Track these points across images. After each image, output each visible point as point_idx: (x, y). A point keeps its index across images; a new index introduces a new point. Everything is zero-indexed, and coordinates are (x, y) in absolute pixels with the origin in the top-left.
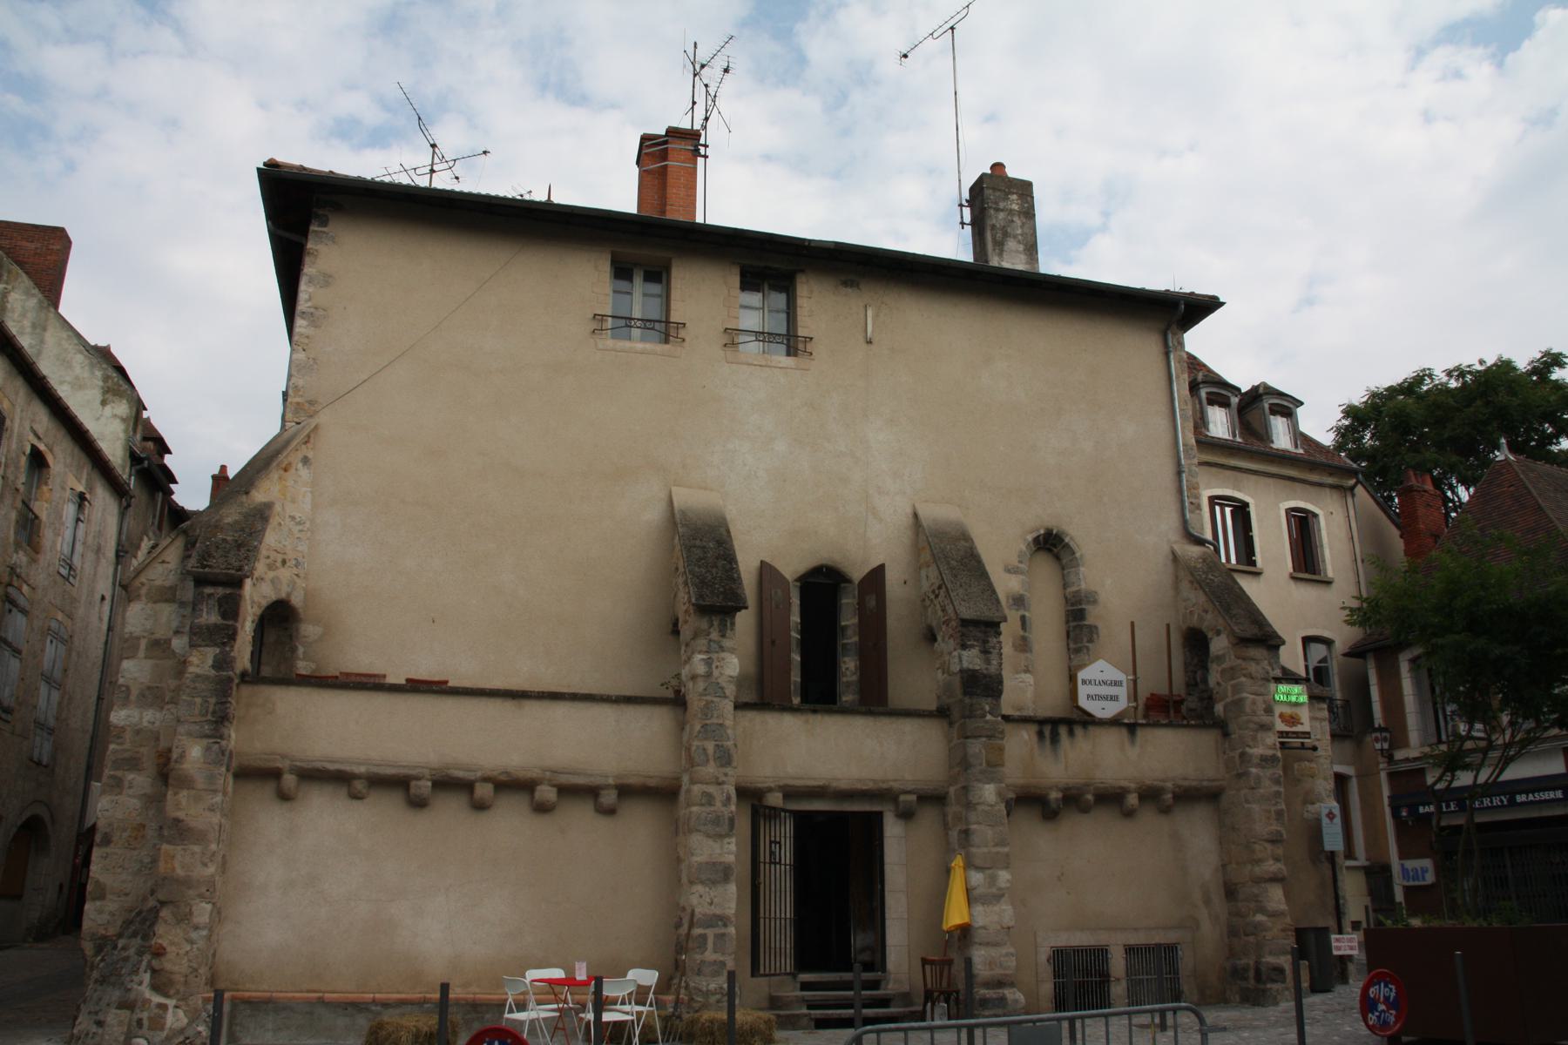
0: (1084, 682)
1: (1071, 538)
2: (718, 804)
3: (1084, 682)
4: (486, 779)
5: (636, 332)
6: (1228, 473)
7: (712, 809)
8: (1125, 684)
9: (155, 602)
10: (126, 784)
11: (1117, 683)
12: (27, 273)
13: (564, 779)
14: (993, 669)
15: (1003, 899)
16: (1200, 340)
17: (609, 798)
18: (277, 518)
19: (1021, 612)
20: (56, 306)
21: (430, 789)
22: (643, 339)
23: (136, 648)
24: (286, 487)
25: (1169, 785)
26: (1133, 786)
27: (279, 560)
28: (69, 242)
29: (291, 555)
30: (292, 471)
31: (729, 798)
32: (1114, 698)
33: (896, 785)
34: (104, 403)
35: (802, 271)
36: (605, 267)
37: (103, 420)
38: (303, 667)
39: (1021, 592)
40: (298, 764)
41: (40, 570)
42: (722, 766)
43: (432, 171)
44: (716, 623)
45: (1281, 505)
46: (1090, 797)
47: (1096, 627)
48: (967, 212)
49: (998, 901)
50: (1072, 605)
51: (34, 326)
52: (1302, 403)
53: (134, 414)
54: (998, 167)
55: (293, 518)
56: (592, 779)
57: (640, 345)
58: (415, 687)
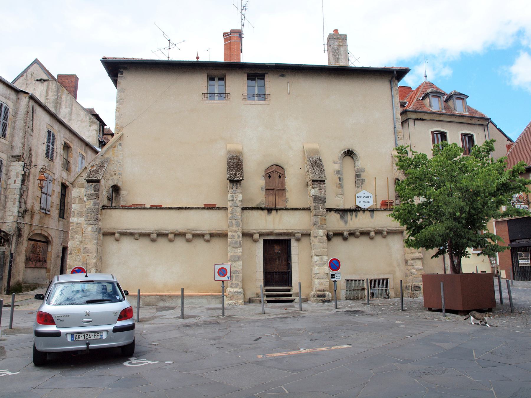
0: (358, 197)
1: (356, 151)
2: (236, 238)
3: (358, 197)
4: (171, 233)
5: (216, 98)
6: (440, 123)
7: (234, 239)
8: (372, 197)
9: (80, 188)
10: (75, 238)
11: (369, 197)
12: (67, 89)
13: (194, 232)
14: (322, 195)
15: (325, 265)
16: (407, 81)
17: (207, 237)
18: (112, 161)
19: (339, 176)
20: (76, 98)
21: (156, 236)
22: (219, 100)
23: (75, 201)
24: (115, 152)
25: (385, 229)
26: (372, 229)
27: (114, 174)
28: (78, 78)
29: (117, 172)
30: (116, 148)
31: (239, 236)
32: (368, 202)
33: (294, 231)
34: (90, 126)
35: (267, 73)
36: (205, 78)
37: (90, 131)
38: (123, 203)
39: (340, 169)
40: (119, 231)
41: (71, 177)
42: (237, 227)
43: (169, 48)
44: (235, 185)
45: (459, 132)
46: (358, 233)
47: (364, 179)
48: (326, 47)
49: (324, 265)
50: (357, 173)
51: (69, 105)
52: (468, 97)
53: (99, 129)
54: (336, 31)
55: (117, 161)
56: (202, 232)
57: (216, 101)
58: (154, 208)
